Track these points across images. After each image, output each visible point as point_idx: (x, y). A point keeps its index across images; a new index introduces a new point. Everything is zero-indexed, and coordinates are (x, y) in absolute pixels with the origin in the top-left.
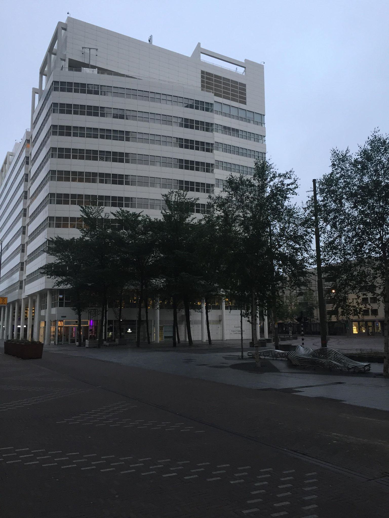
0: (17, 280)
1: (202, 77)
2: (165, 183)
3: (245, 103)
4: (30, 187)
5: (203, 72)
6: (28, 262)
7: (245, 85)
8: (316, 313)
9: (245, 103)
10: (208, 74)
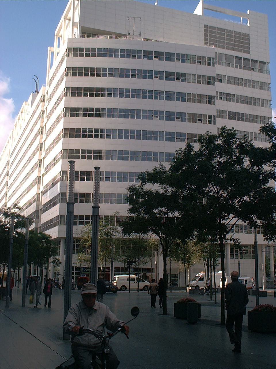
0: (59, 191)
1: (206, 31)
2: (122, 176)
3: (249, 53)
4: (46, 124)
5: (206, 26)
6: (44, 193)
7: (248, 36)
8: (223, 140)
9: (249, 53)
10: (211, 27)
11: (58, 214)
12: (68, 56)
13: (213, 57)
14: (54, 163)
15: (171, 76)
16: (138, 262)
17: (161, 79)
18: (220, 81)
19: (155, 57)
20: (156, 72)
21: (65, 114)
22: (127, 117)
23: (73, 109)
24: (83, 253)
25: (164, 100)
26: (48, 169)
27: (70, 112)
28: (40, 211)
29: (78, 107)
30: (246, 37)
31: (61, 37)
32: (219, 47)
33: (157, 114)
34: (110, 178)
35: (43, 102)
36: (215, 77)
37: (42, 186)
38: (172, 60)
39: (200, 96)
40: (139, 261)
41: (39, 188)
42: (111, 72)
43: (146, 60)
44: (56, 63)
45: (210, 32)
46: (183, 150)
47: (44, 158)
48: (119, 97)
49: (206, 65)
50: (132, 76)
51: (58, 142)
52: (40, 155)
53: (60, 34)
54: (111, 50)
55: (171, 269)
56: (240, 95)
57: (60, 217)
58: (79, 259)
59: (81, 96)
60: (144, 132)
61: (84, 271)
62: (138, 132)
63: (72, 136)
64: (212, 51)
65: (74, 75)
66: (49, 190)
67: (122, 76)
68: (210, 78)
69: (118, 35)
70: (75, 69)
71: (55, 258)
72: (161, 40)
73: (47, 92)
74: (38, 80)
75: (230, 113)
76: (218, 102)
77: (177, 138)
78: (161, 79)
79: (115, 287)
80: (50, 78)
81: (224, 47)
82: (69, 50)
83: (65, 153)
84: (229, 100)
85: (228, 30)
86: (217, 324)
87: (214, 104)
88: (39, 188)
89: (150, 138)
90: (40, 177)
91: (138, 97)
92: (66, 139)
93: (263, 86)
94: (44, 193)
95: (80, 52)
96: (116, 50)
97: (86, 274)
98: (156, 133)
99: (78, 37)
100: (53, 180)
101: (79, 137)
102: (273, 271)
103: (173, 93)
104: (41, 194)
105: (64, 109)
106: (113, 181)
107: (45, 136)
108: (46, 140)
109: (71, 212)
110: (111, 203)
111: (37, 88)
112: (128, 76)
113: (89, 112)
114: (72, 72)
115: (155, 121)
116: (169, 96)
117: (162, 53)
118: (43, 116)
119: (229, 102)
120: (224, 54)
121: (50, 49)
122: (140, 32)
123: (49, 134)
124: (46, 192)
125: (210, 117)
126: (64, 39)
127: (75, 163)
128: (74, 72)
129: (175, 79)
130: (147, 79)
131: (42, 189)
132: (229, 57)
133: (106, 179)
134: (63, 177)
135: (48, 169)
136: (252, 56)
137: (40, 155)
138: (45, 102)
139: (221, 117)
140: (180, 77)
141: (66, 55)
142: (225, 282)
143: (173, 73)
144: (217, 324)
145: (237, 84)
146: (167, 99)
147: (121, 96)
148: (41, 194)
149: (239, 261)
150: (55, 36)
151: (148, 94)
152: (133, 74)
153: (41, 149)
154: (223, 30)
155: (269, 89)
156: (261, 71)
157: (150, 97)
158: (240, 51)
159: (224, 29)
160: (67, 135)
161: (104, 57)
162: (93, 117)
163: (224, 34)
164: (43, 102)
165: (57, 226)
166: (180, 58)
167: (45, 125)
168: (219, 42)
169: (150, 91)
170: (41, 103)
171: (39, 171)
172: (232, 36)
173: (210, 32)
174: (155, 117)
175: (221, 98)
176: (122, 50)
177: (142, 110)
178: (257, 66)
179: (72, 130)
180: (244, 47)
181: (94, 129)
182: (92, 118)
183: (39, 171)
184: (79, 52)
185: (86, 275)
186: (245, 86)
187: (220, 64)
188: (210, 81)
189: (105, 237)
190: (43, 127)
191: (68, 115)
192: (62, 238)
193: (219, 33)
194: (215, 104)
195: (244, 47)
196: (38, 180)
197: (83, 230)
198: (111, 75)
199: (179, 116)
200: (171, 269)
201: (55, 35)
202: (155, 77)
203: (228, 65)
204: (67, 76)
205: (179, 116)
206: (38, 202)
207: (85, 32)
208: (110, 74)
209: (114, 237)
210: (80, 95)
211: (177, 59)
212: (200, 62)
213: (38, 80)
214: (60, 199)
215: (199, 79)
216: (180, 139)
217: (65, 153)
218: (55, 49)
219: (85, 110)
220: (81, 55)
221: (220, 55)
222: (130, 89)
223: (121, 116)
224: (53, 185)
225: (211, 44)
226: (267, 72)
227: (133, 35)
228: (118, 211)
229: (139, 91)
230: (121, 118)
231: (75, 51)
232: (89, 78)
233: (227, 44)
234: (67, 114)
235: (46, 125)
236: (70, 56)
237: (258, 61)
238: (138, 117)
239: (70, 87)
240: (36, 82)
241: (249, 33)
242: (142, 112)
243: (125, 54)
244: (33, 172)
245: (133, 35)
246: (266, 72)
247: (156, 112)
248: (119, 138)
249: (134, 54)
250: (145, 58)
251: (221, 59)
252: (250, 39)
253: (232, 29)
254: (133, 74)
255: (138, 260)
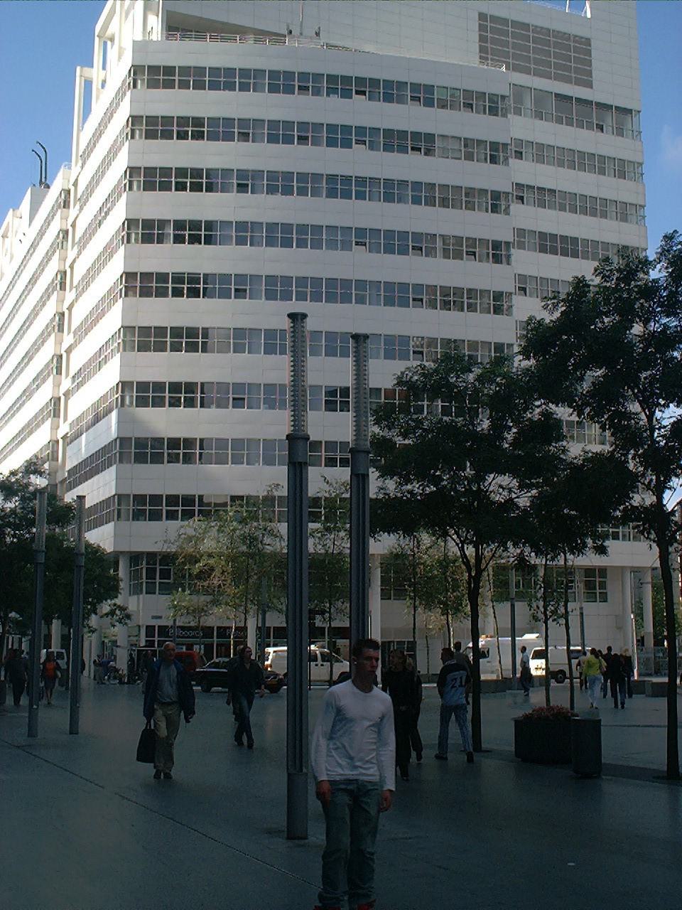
0: (114, 433)
1: (482, 28)
4: (74, 261)
7: (588, 42)
10: (495, 19)
11: (113, 493)
12: (135, 86)
13: (503, 94)
14: (97, 362)
15: (396, 141)
16: (330, 612)
17: (373, 147)
18: (519, 155)
19: (358, 93)
20: (361, 130)
21: (129, 235)
22: (287, 243)
23: (148, 224)
24: (184, 591)
25: (380, 201)
26: (80, 379)
27: (140, 231)
28: (59, 485)
29: (160, 218)
30: (583, 46)
31: (112, 40)
32: (516, 68)
33: (363, 237)
34: (244, 399)
35: (64, 207)
36: (507, 144)
37: (65, 420)
38: (401, 100)
39: (470, 192)
40: (332, 611)
41: (55, 427)
42: (243, 130)
43: (335, 100)
44: (98, 109)
45: (494, 30)
46: (562, 296)
47: (71, 351)
48: (267, 193)
49: (485, 113)
50: (298, 139)
51: (109, 307)
52: (59, 342)
53: (109, 32)
54: (245, 73)
55: (414, 628)
56: (568, 190)
57: (116, 500)
58: (175, 607)
59: (170, 190)
60: (332, 282)
61: (182, 637)
62: (316, 281)
63: (145, 293)
64: (500, 78)
65: (150, 135)
66: (86, 431)
67: (273, 139)
68: (495, 146)
69: (261, 35)
70: (151, 120)
71: (115, 605)
72: (369, 48)
73: (77, 180)
74: (45, 151)
75: (542, 235)
76: (515, 207)
77: (414, 300)
78: (371, 148)
79: (275, 678)
80: (83, 146)
81: (527, 71)
82: (136, 70)
83: (128, 334)
84: (542, 204)
85: (536, 27)
86: (656, 777)
87: (507, 212)
88: (55, 427)
89: (346, 299)
90: (59, 398)
91: (316, 193)
92: (131, 299)
93: (625, 169)
94: (69, 439)
95: (165, 78)
96: (259, 73)
97: (183, 644)
98: (361, 284)
99: (160, 39)
100: (95, 406)
101: (166, 295)
102: (649, 633)
103: (403, 183)
104: (61, 442)
105: (124, 222)
106: (251, 408)
107: (70, 296)
108: (76, 305)
109: (300, 463)
110: (247, 464)
111: (44, 176)
112: (288, 140)
113: (195, 232)
114: (144, 127)
115: (359, 253)
116: (392, 191)
117: (374, 82)
118: (65, 243)
119: (540, 210)
120: (528, 88)
121: (81, 71)
122: (319, 28)
123: (83, 291)
124: (78, 435)
125: (497, 245)
126: (122, 45)
127: (308, 319)
128: (150, 127)
129: (409, 148)
130: (338, 147)
131: (64, 429)
132: (541, 96)
133: (235, 401)
134: (123, 398)
135: (80, 379)
136: (595, 94)
137: (59, 342)
138: (69, 207)
139: (521, 246)
140: (422, 143)
141: (129, 84)
142: (605, 664)
143: (403, 134)
144: (656, 777)
145: (561, 164)
146: (389, 198)
147: (272, 190)
148: (61, 442)
149: (581, 608)
150: (97, 39)
151: (339, 187)
152: (304, 134)
153: (61, 329)
154: (525, 26)
155: (638, 178)
156: (620, 132)
157: (346, 195)
158: (567, 80)
159: (528, 25)
160: (134, 289)
161: (227, 91)
162: (200, 243)
163: (527, 38)
164: (64, 207)
165: (109, 522)
166: (422, 96)
167: (72, 267)
168: (515, 56)
169: (347, 179)
170: (59, 211)
171: (57, 385)
172: (548, 43)
173: (494, 30)
174: (357, 244)
175: (521, 199)
176: (274, 74)
177: (326, 226)
178: (610, 120)
179: (146, 276)
180: (577, 70)
181: (202, 276)
182: (196, 246)
183: (57, 385)
184: (161, 77)
185: (184, 648)
186: (579, 170)
187: (518, 112)
188: (495, 153)
189: (244, 548)
190: (65, 272)
191: (136, 240)
192: (121, 552)
193: (514, 36)
194: (508, 214)
195: (577, 70)
196: (55, 408)
197: (182, 531)
198: (244, 137)
199: (420, 244)
200: (414, 628)
201: (96, 34)
202: (358, 142)
203: (539, 115)
204: (133, 137)
205: (420, 244)
206: (54, 463)
207: (176, 26)
208: (243, 133)
209: (269, 549)
210: (165, 187)
211: (413, 98)
212: (471, 106)
213: (45, 151)
214: (118, 455)
215: (470, 148)
216: (422, 300)
217: (128, 334)
218: (96, 73)
219: (179, 225)
220: (169, 85)
221: (519, 90)
222: (295, 174)
223: (271, 242)
224: (97, 419)
225: (497, 63)
226: (635, 134)
227: (301, 34)
228: (276, 483)
229: (317, 177)
230: (272, 246)
231: (151, 74)
232: (189, 143)
233: (537, 62)
234: (133, 236)
235: (76, 266)
236: (139, 86)
237: (612, 106)
238: (317, 245)
239: (140, 168)
240: (41, 160)
241: (589, 37)
242: (326, 230)
243: (282, 82)
244: (38, 387)
245: (301, 34)
246: (633, 135)
247: (361, 232)
248: (267, 299)
249: (303, 83)
250: (331, 95)
251: (519, 98)
252: (592, 51)
253: (546, 25)
254: (304, 134)
255: (330, 608)
